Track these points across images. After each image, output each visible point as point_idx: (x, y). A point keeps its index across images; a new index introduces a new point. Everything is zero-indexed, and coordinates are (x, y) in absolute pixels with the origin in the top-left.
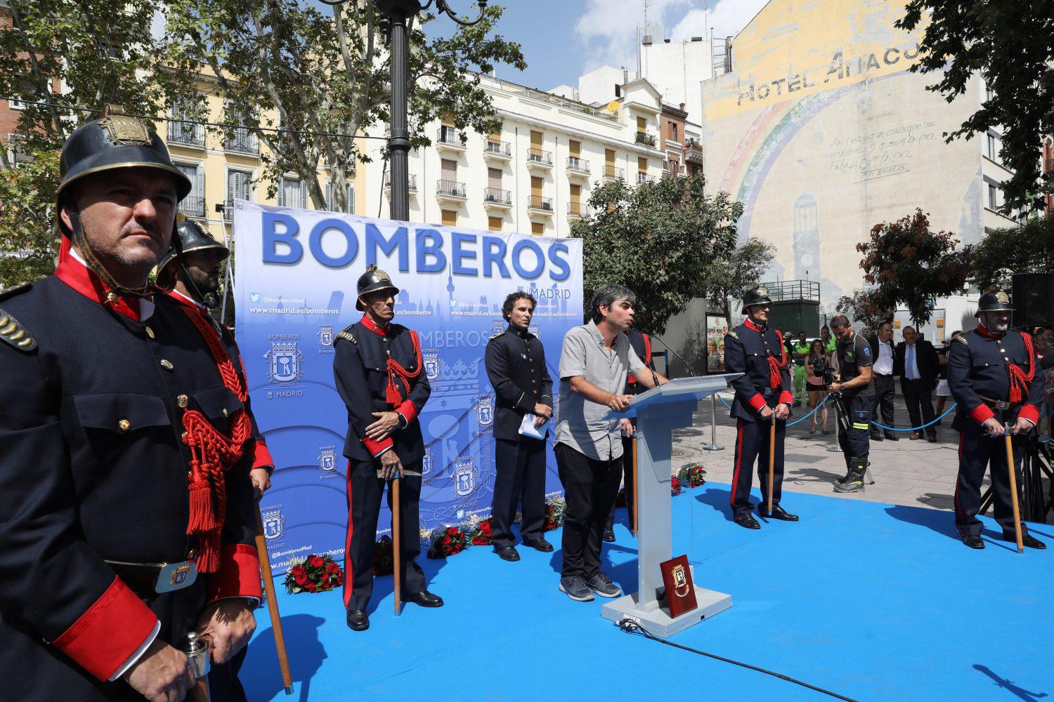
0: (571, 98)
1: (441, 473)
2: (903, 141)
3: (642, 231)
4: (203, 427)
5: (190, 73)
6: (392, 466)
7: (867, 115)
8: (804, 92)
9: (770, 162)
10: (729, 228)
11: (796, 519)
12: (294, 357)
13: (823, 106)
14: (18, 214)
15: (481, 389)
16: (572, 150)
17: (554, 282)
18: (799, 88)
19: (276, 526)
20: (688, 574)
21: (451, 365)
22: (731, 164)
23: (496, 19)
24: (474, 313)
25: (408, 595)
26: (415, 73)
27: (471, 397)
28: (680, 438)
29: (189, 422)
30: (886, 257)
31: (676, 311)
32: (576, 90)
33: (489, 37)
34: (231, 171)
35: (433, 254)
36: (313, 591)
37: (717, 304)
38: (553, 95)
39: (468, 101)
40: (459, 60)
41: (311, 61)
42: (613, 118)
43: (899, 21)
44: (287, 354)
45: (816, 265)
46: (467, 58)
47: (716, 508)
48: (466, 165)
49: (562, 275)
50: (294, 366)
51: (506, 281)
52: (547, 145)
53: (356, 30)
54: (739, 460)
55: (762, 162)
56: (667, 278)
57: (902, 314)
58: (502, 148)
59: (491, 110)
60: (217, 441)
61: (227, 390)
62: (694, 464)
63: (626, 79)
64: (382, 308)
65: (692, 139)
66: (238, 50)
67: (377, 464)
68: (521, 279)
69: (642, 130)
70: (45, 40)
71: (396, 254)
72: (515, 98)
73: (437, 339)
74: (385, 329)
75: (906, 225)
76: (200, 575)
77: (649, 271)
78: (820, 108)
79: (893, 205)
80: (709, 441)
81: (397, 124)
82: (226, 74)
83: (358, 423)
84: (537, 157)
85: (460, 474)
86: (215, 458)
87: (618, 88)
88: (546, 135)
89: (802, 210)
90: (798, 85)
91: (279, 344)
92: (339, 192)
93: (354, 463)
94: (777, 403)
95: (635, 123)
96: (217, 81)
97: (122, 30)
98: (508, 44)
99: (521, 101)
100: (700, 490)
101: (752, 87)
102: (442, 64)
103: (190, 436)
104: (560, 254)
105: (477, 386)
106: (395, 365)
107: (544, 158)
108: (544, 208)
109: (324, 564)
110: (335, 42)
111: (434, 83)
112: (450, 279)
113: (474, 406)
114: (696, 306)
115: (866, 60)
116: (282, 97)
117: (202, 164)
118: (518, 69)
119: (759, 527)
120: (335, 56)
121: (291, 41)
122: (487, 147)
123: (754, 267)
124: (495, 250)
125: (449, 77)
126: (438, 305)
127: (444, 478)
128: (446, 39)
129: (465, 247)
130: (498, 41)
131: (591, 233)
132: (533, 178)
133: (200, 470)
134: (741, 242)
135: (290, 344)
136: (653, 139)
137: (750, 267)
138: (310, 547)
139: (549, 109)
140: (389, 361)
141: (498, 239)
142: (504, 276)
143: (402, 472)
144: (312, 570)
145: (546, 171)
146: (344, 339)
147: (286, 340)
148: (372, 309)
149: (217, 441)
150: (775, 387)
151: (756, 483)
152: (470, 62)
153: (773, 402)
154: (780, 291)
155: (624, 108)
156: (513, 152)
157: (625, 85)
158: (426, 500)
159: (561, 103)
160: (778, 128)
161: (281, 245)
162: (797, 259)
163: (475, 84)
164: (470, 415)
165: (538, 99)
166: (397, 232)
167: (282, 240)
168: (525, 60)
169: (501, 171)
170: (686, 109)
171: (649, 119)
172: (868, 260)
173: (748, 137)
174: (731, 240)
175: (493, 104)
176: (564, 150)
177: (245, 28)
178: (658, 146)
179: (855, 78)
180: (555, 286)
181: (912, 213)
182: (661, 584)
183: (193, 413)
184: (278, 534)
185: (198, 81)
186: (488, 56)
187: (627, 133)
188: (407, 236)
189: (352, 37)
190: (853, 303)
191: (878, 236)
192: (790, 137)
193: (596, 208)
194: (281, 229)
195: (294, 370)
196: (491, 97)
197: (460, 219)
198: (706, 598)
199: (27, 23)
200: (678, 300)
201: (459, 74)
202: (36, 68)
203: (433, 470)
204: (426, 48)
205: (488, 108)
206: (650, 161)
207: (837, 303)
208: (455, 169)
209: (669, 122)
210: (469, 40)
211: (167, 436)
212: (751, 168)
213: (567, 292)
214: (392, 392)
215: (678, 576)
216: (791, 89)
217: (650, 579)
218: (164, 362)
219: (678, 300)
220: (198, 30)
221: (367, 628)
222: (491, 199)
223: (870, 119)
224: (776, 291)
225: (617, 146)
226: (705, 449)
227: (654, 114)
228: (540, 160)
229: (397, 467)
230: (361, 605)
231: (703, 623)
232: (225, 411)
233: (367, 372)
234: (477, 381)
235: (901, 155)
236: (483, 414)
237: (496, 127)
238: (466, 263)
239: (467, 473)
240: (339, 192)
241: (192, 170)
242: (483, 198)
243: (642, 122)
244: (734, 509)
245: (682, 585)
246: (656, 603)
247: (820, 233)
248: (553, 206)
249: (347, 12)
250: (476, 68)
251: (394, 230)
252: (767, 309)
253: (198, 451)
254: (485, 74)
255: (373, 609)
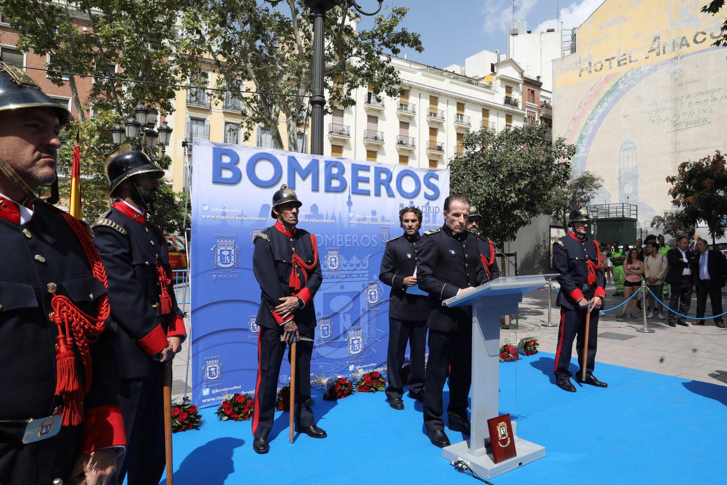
0: (460, 74)
1: (338, 337)
2: (706, 101)
3: (500, 164)
4: (69, 308)
5: (197, 58)
6: (291, 333)
7: (678, 81)
8: (629, 66)
9: (602, 117)
10: (565, 164)
11: (605, 386)
12: (233, 250)
13: (643, 77)
14: (88, 150)
15: (370, 278)
16: (458, 109)
17: (427, 201)
18: (625, 64)
19: (215, 370)
20: (509, 429)
21: (348, 260)
22: (572, 119)
23: (403, 17)
24: (366, 222)
25: (301, 428)
26: (346, 55)
27: (362, 283)
28: (526, 316)
29: (57, 304)
30: (690, 187)
31: (524, 224)
32: (463, 69)
33: (397, 29)
34: (227, 123)
35: (337, 179)
36: (237, 419)
37: (559, 219)
38: (446, 71)
39: (382, 74)
40: (376, 46)
41: (277, 48)
42: (488, 87)
43: (706, 7)
44: (228, 248)
45: (635, 193)
46: (382, 44)
47: (544, 373)
48: (384, 119)
49: (433, 196)
50: (233, 257)
51: (391, 199)
52: (441, 106)
53: (306, 26)
54: (562, 339)
55: (596, 118)
56: (516, 200)
57: (702, 229)
58: (410, 108)
59: (398, 80)
60: (81, 320)
61: (96, 279)
62: (530, 338)
63: (499, 59)
64: (289, 215)
65: (545, 102)
66: (227, 40)
67: (281, 330)
68: (402, 198)
69: (509, 95)
70: (108, 39)
71: (309, 179)
72: (420, 73)
73: (338, 240)
74: (292, 232)
75: (707, 163)
76: (63, 428)
77: (503, 194)
78: (641, 78)
79: (697, 149)
80: (546, 320)
81: (316, 86)
82: (220, 57)
83: (269, 302)
84: (434, 114)
85: (353, 338)
86: (80, 332)
87: (493, 66)
88: (440, 99)
89: (626, 152)
90: (624, 62)
91: (222, 241)
92: (292, 137)
93: (264, 329)
94: (593, 296)
95: (504, 90)
96: (213, 62)
97: (157, 31)
98: (411, 34)
99: (424, 75)
100: (534, 358)
101: (590, 64)
102: (364, 48)
103: (57, 315)
104: (432, 181)
105: (367, 275)
106: (299, 260)
107: (439, 115)
108: (438, 150)
109: (246, 400)
110: (293, 35)
111: (359, 62)
112: (350, 197)
113: (364, 289)
114: (542, 220)
115: (679, 41)
116: (256, 73)
117: (208, 119)
118: (417, 52)
119: (575, 391)
120: (292, 44)
121: (263, 35)
122: (399, 107)
123: (586, 193)
124: (384, 176)
125: (369, 57)
126: (340, 215)
127: (337, 340)
128: (367, 31)
129: (361, 174)
130: (404, 32)
131: (463, 166)
132: (431, 129)
133: (65, 342)
134: (576, 173)
135: (230, 241)
136: (517, 101)
137: (583, 193)
138: (240, 387)
139: (443, 80)
140: (294, 256)
141: (386, 169)
142: (389, 196)
143: (298, 337)
144: (236, 405)
145: (440, 124)
146: (261, 238)
147: (228, 238)
148: (281, 216)
149: (81, 320)
150: (591, 283)
151: (574, 355)
152: (384, 47)
153: (589, 295)
154: (607, 211)
155: (496, 80)
156: (417, 111)
157: (497, 63)
158: (327, 357)
159: (452, 77)
160: (609, 93)
161: (225, 169)
162: (621, 188)
163: (388, 62)
164: (361, 296)
165: (436, 74)
166: (311, 162)
167: (227, 167)
168: (423, 45)
169: (408, 124)
170: (541, 80)
171: (514, 87)
172: (675, 189)
173: (586, 99)
174: (566, 172)
175: (400, 76)
176: (453, 110)
177: (232, 26)
178: (520, 106)
179: (669, 55)
180: (428, 203)
181: (712, 155)
182: (488, 436)
183: (60, 298)
184: (217, 376)
185: (201, 62)
186: (397, 43)
187: (498, 97)
188: (318, 166)
189: (304, 31)
190: (663, 221)
191: (684, 171)
192: (617, 99)
193: (467, 148)
194: (226, 159)
195: (233, 260)
196: (398, 72)
197: (379, 157)
198: (524, 448)
199: (97, 28)
200: (525, 216)
201: (376, 55)
202: (102, 56)
203: (332, 335)
204: (354, 37)
205: (396, 79)
206: (514, 117)
207: (651, 220)
208: (343, 116)
209: (529, 90)
210: (383, 32)
211: (37, 317)
212: (588, 121)
213: (437, 209)
214: (294, 280)
215: (502, 430)
216: (619, 64)
217: (479, 429)
218: (37, 257)
219: (525, 216)
220: (199, 29)
221: (266, 452)
222: (401, 143)
223: (680, 85)
224: (604, 211)
225: (491, 107)
226: (543, 325)
227: (517, 84)
228: (436, 116)
229: (295, 334)
230: (263, 434)
231: (521, 468)
232: (91, 296)
233: (277, 263)
234: (367, 272)
235: (705, 112)
236: (371, 295)
237: (404, 93)
238: (362, 186)
239: (357, 338)
240: (292, 137)
241: (202, 122)
242: (395, 141)
243: (509, 90)
244: (557, 375)
245: (505, 438)
246: (484, 449)
247: (639, 169)
248: (444, 148)
249: (302, 14)
250: (389, 51)
251: (309, 161)
252: (586, 225)
253: (63, 326)
254: (395, 55)
255: (274, 437)
